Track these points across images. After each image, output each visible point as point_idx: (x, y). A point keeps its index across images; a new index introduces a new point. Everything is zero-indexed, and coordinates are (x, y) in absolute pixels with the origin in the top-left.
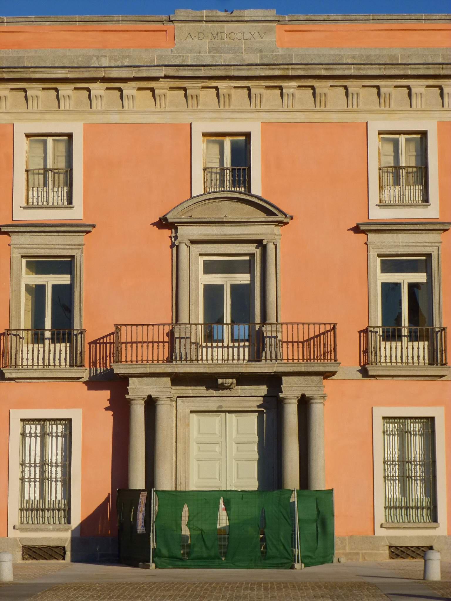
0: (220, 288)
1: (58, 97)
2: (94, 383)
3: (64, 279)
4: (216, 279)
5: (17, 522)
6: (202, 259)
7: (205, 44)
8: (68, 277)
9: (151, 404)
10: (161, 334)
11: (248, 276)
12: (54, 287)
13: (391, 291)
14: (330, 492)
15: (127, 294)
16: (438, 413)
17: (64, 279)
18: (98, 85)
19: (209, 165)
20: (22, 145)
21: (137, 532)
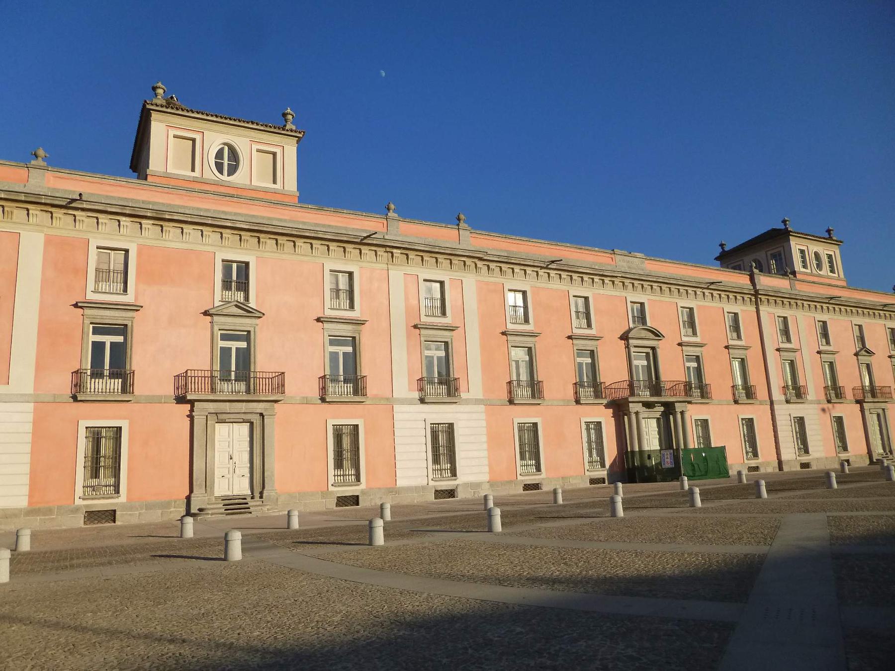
0: (104, 343)
1: (98, 223)
2: (607, 406)
3: (120, 339)
4: (99, 338)
5: (81, 494)
6: (220, 332)
7: (625, 264)
8: (245, 343)
9: (637, 413)
10: (626, 385)
11: (245, 343)
12: (237, 349)
13: (98, 348)
14: (723, 449)
15: (613, 371)
16: (125, 425)
17: (120, 339)
18: (228, 231)
19: (101, 266)
20: (93, 253)
21: (672, 468)
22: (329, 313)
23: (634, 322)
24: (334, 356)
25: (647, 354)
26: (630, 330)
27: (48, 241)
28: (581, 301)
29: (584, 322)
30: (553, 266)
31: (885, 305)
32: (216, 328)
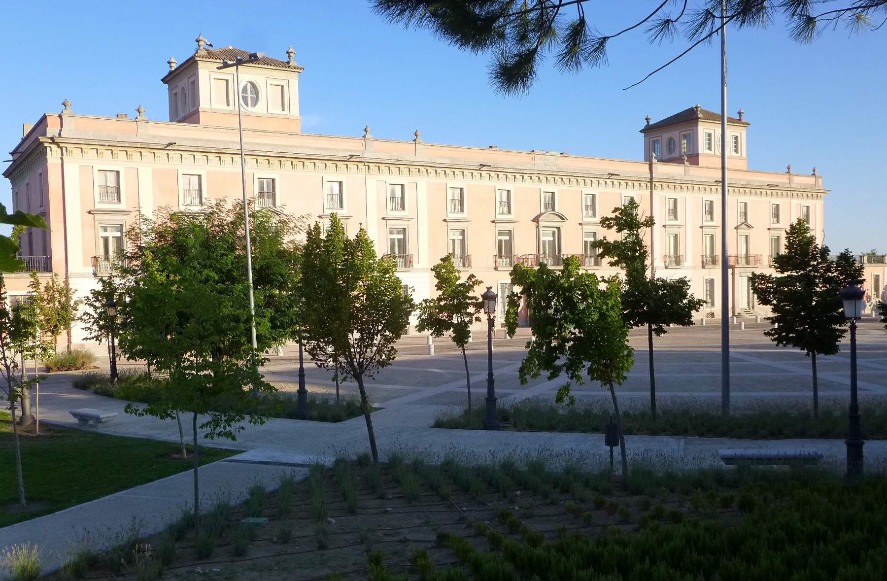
7: (542, 162)
22: (99, 206)
23: (545, 207)
24: (392, 242)
25: (554, 232)
26: (541, 215)
27: (155, 173)
28: (505, 193)
29: (506, 209)
30: (485, 168)
31: (352, 156)
32: (97, 223)
